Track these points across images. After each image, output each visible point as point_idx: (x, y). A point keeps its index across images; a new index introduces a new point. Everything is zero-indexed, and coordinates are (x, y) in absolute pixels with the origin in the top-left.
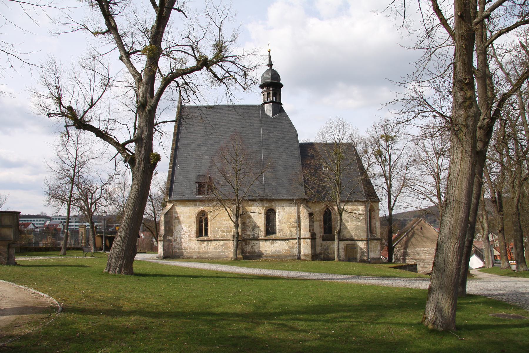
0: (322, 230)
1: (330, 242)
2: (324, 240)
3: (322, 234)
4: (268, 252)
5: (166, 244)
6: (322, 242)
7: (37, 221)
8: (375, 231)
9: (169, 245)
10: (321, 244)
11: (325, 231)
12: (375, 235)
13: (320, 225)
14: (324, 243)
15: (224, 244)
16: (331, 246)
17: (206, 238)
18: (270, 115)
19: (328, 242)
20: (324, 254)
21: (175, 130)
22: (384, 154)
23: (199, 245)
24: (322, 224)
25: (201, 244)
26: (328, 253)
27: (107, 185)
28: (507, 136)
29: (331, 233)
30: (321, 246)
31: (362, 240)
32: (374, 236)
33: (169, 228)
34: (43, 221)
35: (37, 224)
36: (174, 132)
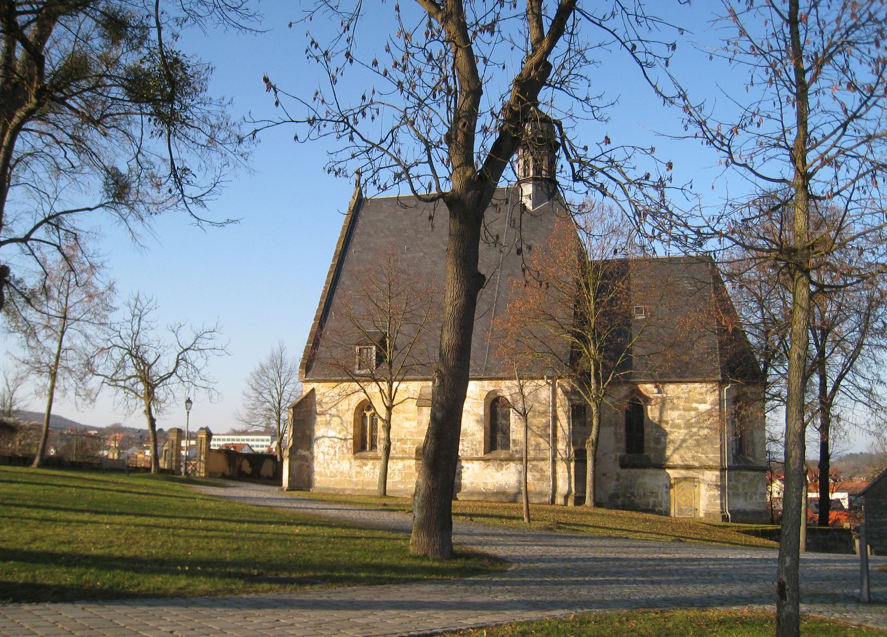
0: (623, 445)
1: (638, 471)
2: (623, 466)
3: (619, 454)
4: (489, 487)
5: (296, 464)
6: (619, 470)
7: (258, 440)
8: (750, 450)
9: (301, 466)
10: (618, 475)
11: (628, 446)
12: (750, 459)
13: (615, 433)
14: (624, 472)
15: (404, 467)
16: (641, 480)
17: (370, 454)
18: (531, 208)
19: (633, 471)
20: (625, 496)
21: (338, 247)
22: (71, 155)
23: (358, 469)
24: (622, 431)
25: (361, 467)
26: (632, 494)
27: (190, 352)
28: (836, 162)
29: (643, 452)
30: (618, 480)
31: (710, 468)
32: (747, 461)
33: (303, 434)
34: (267, 440)
35: (257, 446)
36: (336, 251)
